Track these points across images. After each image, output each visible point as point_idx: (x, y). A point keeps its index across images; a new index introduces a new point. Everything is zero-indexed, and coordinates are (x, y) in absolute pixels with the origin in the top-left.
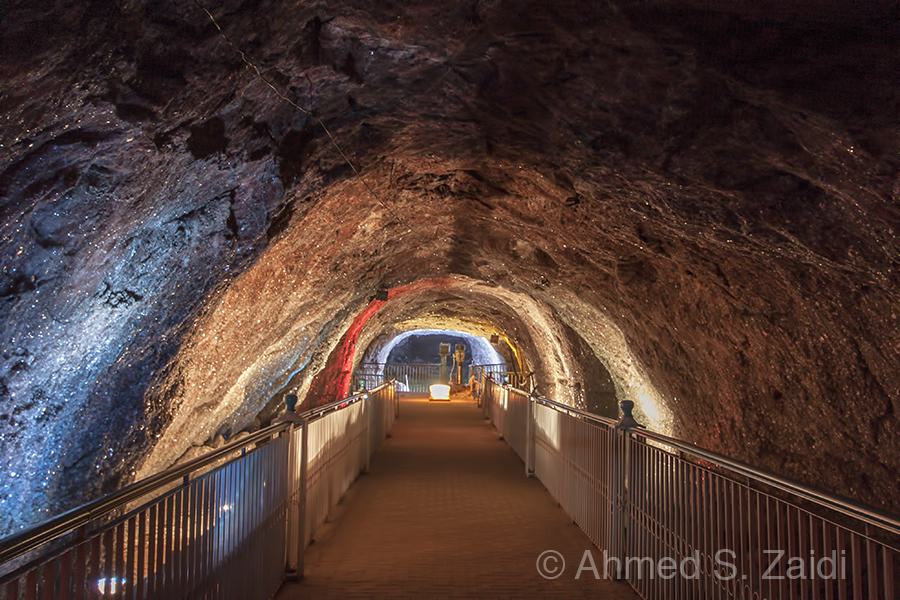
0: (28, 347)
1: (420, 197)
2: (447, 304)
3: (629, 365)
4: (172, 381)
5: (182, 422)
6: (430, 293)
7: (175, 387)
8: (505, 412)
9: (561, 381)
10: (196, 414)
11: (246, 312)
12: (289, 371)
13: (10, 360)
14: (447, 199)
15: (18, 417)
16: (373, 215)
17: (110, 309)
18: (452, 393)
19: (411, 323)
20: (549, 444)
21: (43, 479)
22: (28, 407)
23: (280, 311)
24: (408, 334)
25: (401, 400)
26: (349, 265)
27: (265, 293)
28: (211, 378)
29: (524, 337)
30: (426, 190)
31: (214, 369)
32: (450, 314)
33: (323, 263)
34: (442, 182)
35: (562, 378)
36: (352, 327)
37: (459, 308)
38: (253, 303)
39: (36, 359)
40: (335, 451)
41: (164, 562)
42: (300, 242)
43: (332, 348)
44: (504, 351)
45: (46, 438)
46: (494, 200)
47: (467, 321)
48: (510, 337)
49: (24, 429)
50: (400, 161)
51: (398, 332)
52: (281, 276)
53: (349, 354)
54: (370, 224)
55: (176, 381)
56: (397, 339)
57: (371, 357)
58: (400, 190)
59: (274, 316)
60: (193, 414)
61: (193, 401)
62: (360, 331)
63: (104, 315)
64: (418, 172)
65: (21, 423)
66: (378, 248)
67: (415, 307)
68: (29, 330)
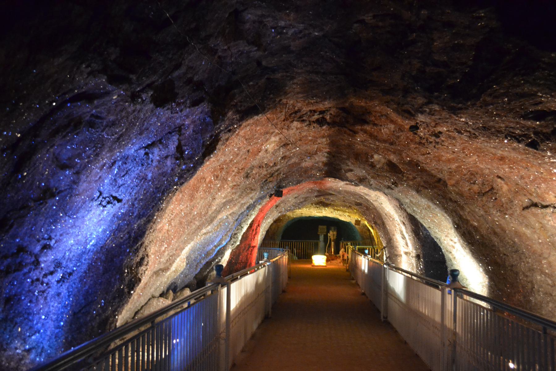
1: (306, 126)
4: (140, 255)
6: (312, 191)
8: (367, 275)
9: (406, 253)
10: (155, 276)
11: (187, 207)
12: (216, 247)
14: (324, 127)
15: (46, 280)
16: (273, 139)
17: (101, 208)
18: (327, 260)
22: (52, 273)
23: (210, 205)
27: (200, 194)
28: (164, 251)
29: (379, 222)
30: (310, 121)
31: (166, 246)
32: (325, 205)
34: (321, 116)
35: (407, 251)
37: (332, 201)
38: (191, 201)
39: (56, 242)
47: (338, 210)
48: (369, 222)
49: (49, 287)
50: (292, 102)
52: (211, 182)
53: (256, 234)
54: (272, 143)
55: (143, 255)
58: (292, 122)
60: (153, 276)
62: (263, 218)
63: (98, 212)
64: (304, 109)
65: (47, 284)
67: (302, 200)
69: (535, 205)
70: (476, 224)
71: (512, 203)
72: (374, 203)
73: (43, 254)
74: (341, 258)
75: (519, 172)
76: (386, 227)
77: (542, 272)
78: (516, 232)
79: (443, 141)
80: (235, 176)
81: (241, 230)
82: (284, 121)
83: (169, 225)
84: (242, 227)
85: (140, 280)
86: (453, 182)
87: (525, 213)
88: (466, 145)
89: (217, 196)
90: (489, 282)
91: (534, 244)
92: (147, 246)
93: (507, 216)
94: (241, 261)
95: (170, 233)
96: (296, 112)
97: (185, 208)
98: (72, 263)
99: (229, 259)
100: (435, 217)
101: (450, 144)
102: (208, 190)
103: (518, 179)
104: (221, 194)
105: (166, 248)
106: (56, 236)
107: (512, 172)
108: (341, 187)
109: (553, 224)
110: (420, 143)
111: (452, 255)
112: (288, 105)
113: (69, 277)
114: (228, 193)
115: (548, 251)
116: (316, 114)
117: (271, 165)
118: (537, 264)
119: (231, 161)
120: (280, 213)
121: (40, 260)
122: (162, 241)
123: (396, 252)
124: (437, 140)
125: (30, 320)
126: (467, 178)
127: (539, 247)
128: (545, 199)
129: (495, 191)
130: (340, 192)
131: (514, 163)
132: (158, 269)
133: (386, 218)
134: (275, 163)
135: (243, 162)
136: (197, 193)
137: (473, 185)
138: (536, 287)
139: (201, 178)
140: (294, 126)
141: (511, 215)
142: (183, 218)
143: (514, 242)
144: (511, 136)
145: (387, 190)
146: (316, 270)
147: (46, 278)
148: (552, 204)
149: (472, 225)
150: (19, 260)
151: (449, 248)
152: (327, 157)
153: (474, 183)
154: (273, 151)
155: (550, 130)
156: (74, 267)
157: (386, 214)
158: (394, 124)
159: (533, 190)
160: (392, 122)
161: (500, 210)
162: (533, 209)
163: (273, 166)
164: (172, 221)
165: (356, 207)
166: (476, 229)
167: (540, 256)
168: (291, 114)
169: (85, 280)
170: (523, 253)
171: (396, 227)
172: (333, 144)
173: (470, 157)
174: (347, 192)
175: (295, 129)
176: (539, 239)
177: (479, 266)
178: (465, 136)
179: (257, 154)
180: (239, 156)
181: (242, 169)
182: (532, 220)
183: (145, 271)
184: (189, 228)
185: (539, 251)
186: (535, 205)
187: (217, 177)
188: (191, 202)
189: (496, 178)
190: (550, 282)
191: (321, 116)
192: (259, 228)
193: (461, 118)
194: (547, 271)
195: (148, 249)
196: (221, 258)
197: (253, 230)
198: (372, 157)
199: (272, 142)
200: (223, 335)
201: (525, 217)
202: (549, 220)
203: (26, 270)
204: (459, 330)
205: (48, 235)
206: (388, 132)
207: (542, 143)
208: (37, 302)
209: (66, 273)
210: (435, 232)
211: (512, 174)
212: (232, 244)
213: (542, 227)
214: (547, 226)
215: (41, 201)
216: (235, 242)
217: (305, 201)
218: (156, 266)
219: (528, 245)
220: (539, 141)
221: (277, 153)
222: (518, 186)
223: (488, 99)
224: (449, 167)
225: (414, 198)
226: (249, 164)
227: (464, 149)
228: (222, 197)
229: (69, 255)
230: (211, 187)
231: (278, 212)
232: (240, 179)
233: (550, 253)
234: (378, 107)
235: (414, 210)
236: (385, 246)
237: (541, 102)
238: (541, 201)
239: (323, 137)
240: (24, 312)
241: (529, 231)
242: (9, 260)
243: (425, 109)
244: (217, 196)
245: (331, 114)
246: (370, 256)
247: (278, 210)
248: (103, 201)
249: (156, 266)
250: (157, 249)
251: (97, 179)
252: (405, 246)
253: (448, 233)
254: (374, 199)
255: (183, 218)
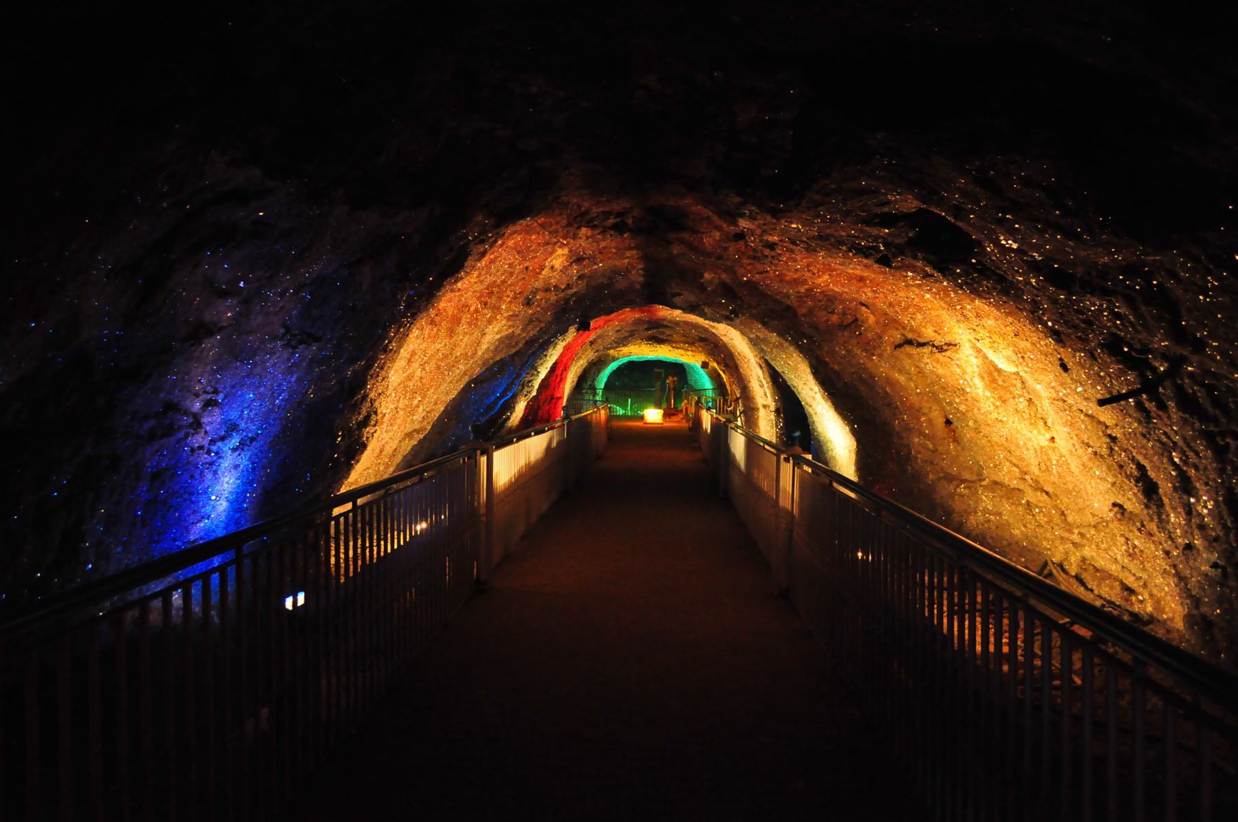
0: (217, 386)
1: (599, 234)
2: (657, 333)
3: (816, 393)
4: (364, 411)
5: (394, 447)
6: (638, 322)
7: (368, 418)
8: (709, 435)
9: (765, 406)
10: (407, 439)
11: (445, 345)
12: (499, 398)
13: (201, 398)
14: (626, 235)
15: (214, 448)
16: (560, 251)
17: (290, 350)
18: (666, 415)
19: (625, 350)
20: (738, 468)
21: (244, 501)
22: (222, 439)
23: (479, 343)
24: (625, 360)
25: (615, 423)
26: (542, 300)
27: (463, 327)
28: (417, 406)
29: (731, 364)
30: (604, 227)
31: (420, 399)
32: (660, 341)
33: (515, 298)
34: (619, 220)
35: (765, 403)
36: (562, 356)
37: (668, 335)
38: (451, 337)
39: (226, 397)
40: (529, 478)
41: (967, 637)
42: (489, 279)
43: (542, 375)
44: (715, 377)
45: (242, 466)
46: (672, 236)
47: (678, 348)
48: (719, 364)
49: (220, 458)
50: (575, 201)
51: (614, 359)
52: (476, 311)
53: (561, 381)
54: (559, 258)
55: (368, 412)
56: (613, 366)
57: (589, 383)
58: (579, 228)
59: (473, 348)
60: (404, 439)
61: (402, 428)
62: (572, 359)
63: (286, 355)
64: (594, 210)
65: (217, 453)
66: (570, 282)
67: (626, 335)
68: (216, 371)
69: (909, 342)
70: (836, 367)
71: (881, 340)
72: (723, 338)
73: (206, 413)
74: (684, 413)
75: (886, 297)
76: (739, 370)
77: (921, 433)
78: (888, 379)
79: (780, 255)
80: (510, 302)
81: (538, 375)
82: (567, 226)
83: (422, 371)
84: (539, 372)
85: (364, 446)
86: (804, 311)
87: (898, 352)
88: (811, 260)
89: (487, 330)
90: (857, 447)
91: (911, 395)
92: (375, 400)
93: (874, 358)
94: (541, 417)
95: (424, 381)
96: (583, 215)
97: (442, 347)
98: (255, 425)
99: (523, 415)
100: (789, 357)
101: (789, 258)
102: (473, 323)
103: (885, 307)
104: (493, 328)
105: (420, 401)
106: (225, 388)
107: (878, 298)
108: (677, 316)
109: (932, 368)
110: (755, 258)
111: (813, 409)
112: (570, 204)
113: (251, 443)
114: (503, 327)
115: (929, 405)
116: (612, 217)
117: (563, 287)
118: (914, 421)
119: (504, 282)
120: (597, 351)
121: (202, 421)
122: (414, 393)
123: (752, 405)
124: (773, 253)
125: (193, 502)
126: (823, 305)
127: (916, 399)
128: (921, 334)
129: (859, 323)
130: (677, 323)
131: (878, 285)
132: (410, 430)
133: (739, 359)
134: (568, 285)
135: (520, 283)
136: (458, 326)
137: (830, 315)
138: (913, 452)
139: (463, 306)
140: (582, 234)
141: (880, 356)
142: (442, 360)
143: (886, 393)
144: (856, 249)
145: (728, 319)
146: (647, 429)
147: (214, 445)
148: (931, 341)
149: (832, 369)
150: (167, 422)
151: (809, 400)
152: (643, 276)
153: (833, 312)
154: (561, 267)
155: (903, 240)
156: (258, 429)
157: (738, 353)
158: (719, 231)
159: (906, 322)
160: (718, 228)
161: (866, 349)
162: (908, 349)
163: (565, 289)
164: (426, 365)
165: (702, 344)
166: (837, 373)
167: (918, 411)
168: (576, 217)
169: (278, 447)
170: (897, 407)
171: (752, 370)
172: (646, 258)
173: (819, 277)
174: (686, 323)
175: (584, 238)
176: (917, 388)
177: (844, 425)
178: (802, 247)
179: (540, 273)
180: (515, 276)
181: (520, 293)
182: (907, 362)
183: (373, 433)
184: (450, 374)
185: (917, 404)
186: (909, 342)
187: (486, 304)
188: (451, 339)
189: (859, 306)
190: (931, 446)
191: (619, 220)
192: (565, 373)
193: (792, 223)
194: (927, 432)
195: (377, 404)
196: (511, 413)
197: (557, 376)
198: (702, 276)
199: (559, 256)
200: (483, 519)
201: (897, 358)
202: (927, 363)
203: (181, 434)
204: (796, 511)
205: (212, 387)
206: (711, 242)
207: (894, 258)
208: (201, 477)
209: (246, 438)
210: (790, 378)
211: (877, 300)
212: (526, 395)
213: (920, 372)
214: (925, 370)
215: (192, 342)
216: (529, 392)
217: (631, 336)
218: (407, 425)
219: (903, 397)
220: (890, 256)
221: (569, 271)
222: (886, 316)
223: (817, 197)
224: (796, 290)
225: (760, 332)
226: (530, 286)
227: (809, 266)
228: (494, 331)
229: (248, 414)
230: (477, 319)
231: (594, 351)
232: (518, 308)
233: (931, 408)
234: (694, 206)
235: (762, 349)
236: (738, 396)
237: (888, 202)
238: (917, 337)
239: (631, 249)
240: (182, 492)
241: (903, 378)
242: (152, 422)
243: (744, 211)
244: (487, 330)
245: (634, 217)
246: (714, 411)
247: (593, 349)
248: (292, 340)
249: (407, 425)
250: (407, 403)
251: (278, 309)
252: (764, 397)
253: (807, 380)
254: (723, 333)
255: (442, 360)
